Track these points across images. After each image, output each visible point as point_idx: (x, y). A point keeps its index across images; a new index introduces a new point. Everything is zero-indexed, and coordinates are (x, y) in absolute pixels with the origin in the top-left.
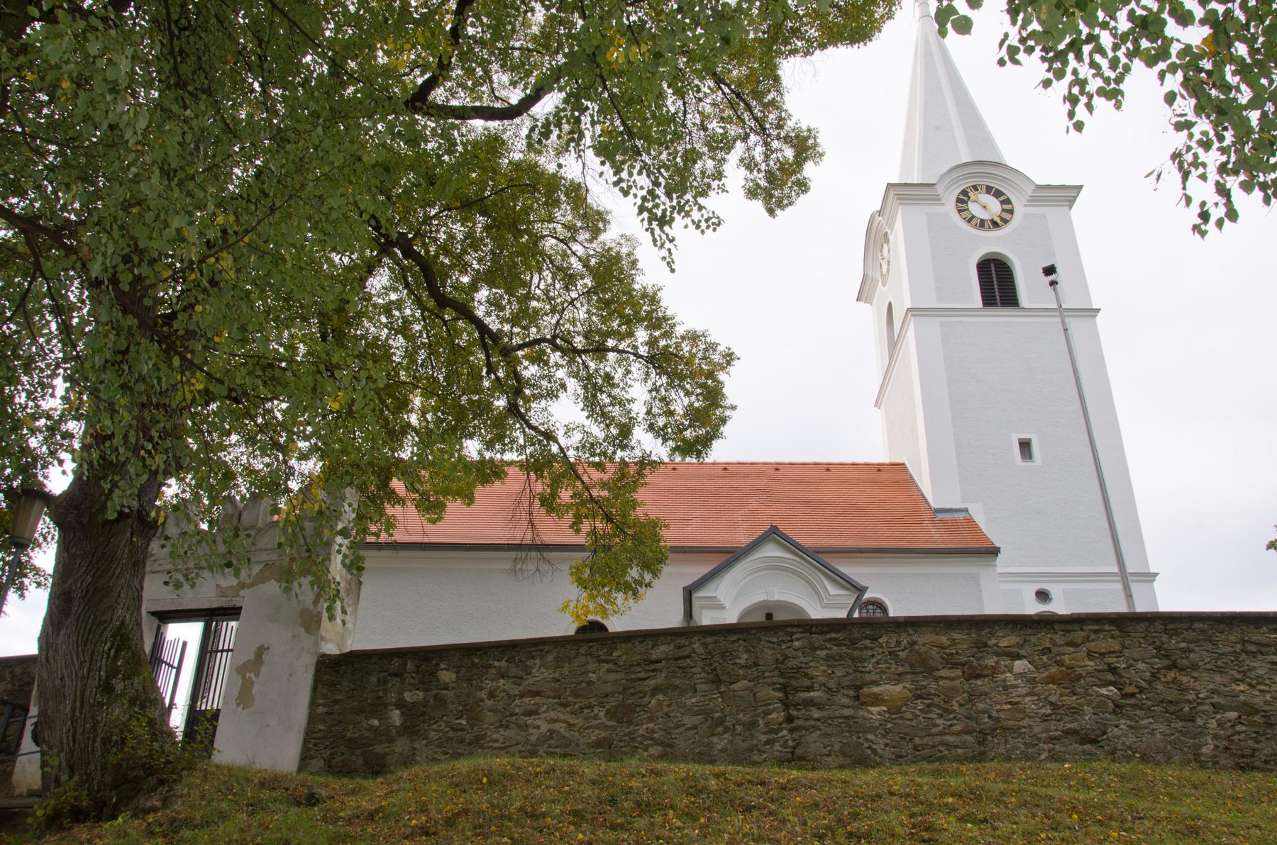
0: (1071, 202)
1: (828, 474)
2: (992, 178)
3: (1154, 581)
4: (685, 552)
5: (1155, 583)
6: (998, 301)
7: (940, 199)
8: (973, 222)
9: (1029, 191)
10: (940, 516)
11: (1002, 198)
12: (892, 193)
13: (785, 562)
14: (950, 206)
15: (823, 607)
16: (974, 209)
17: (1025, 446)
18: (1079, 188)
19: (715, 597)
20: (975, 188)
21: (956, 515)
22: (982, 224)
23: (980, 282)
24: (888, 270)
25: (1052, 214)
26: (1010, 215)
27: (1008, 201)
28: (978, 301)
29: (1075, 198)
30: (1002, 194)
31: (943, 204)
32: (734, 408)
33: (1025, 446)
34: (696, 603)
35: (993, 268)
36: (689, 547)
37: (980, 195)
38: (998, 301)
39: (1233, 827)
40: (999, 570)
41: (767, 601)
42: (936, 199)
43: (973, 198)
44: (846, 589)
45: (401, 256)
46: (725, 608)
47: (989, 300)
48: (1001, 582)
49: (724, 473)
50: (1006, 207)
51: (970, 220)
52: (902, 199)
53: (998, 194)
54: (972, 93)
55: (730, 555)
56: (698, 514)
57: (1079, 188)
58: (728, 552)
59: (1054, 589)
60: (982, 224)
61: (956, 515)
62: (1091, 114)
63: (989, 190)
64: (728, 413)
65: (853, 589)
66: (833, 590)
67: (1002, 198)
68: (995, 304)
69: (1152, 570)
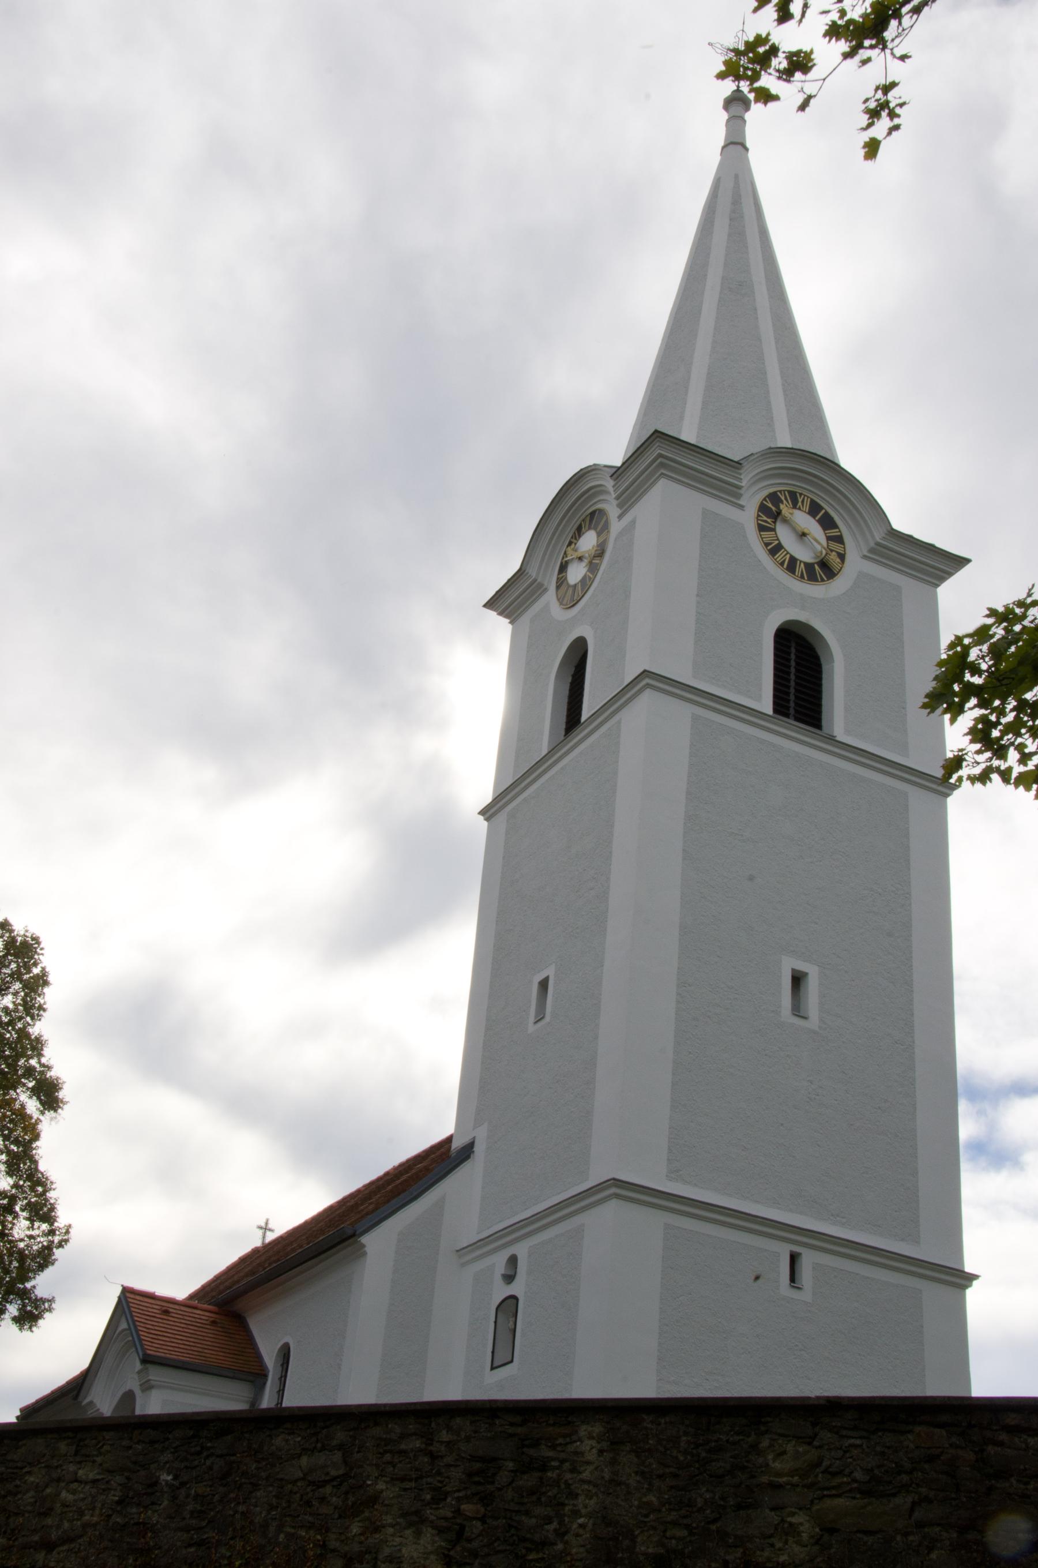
0: (942, 576)
2: (826, 491)
3: (948, 795)
5: (950, 800)
6: (792, 711)
7: (739, 496)
8: (779, 556)
9: (878, 536)
11: (833, 532)
14: (747, 517)
16: (784, 535)
22: (791, 565)
23: (776, 669)
25: (909, 586)
27: (839, 539)
28: (766, 704)
30: (835, 526)
31: (741, 507)
35: (793, 650)
37: (796, 512)
38: (792, 711)
42: (731, 493)
45: (992, 641)
47: (781, 706)
50: (834, 546)
51: (775, 549)
53: (827, 523)
54: (774, 245)
62: (920, 708)
63: (814, 509)
67: (833, 532)
68: (787, 715)
69: (968, 1268)
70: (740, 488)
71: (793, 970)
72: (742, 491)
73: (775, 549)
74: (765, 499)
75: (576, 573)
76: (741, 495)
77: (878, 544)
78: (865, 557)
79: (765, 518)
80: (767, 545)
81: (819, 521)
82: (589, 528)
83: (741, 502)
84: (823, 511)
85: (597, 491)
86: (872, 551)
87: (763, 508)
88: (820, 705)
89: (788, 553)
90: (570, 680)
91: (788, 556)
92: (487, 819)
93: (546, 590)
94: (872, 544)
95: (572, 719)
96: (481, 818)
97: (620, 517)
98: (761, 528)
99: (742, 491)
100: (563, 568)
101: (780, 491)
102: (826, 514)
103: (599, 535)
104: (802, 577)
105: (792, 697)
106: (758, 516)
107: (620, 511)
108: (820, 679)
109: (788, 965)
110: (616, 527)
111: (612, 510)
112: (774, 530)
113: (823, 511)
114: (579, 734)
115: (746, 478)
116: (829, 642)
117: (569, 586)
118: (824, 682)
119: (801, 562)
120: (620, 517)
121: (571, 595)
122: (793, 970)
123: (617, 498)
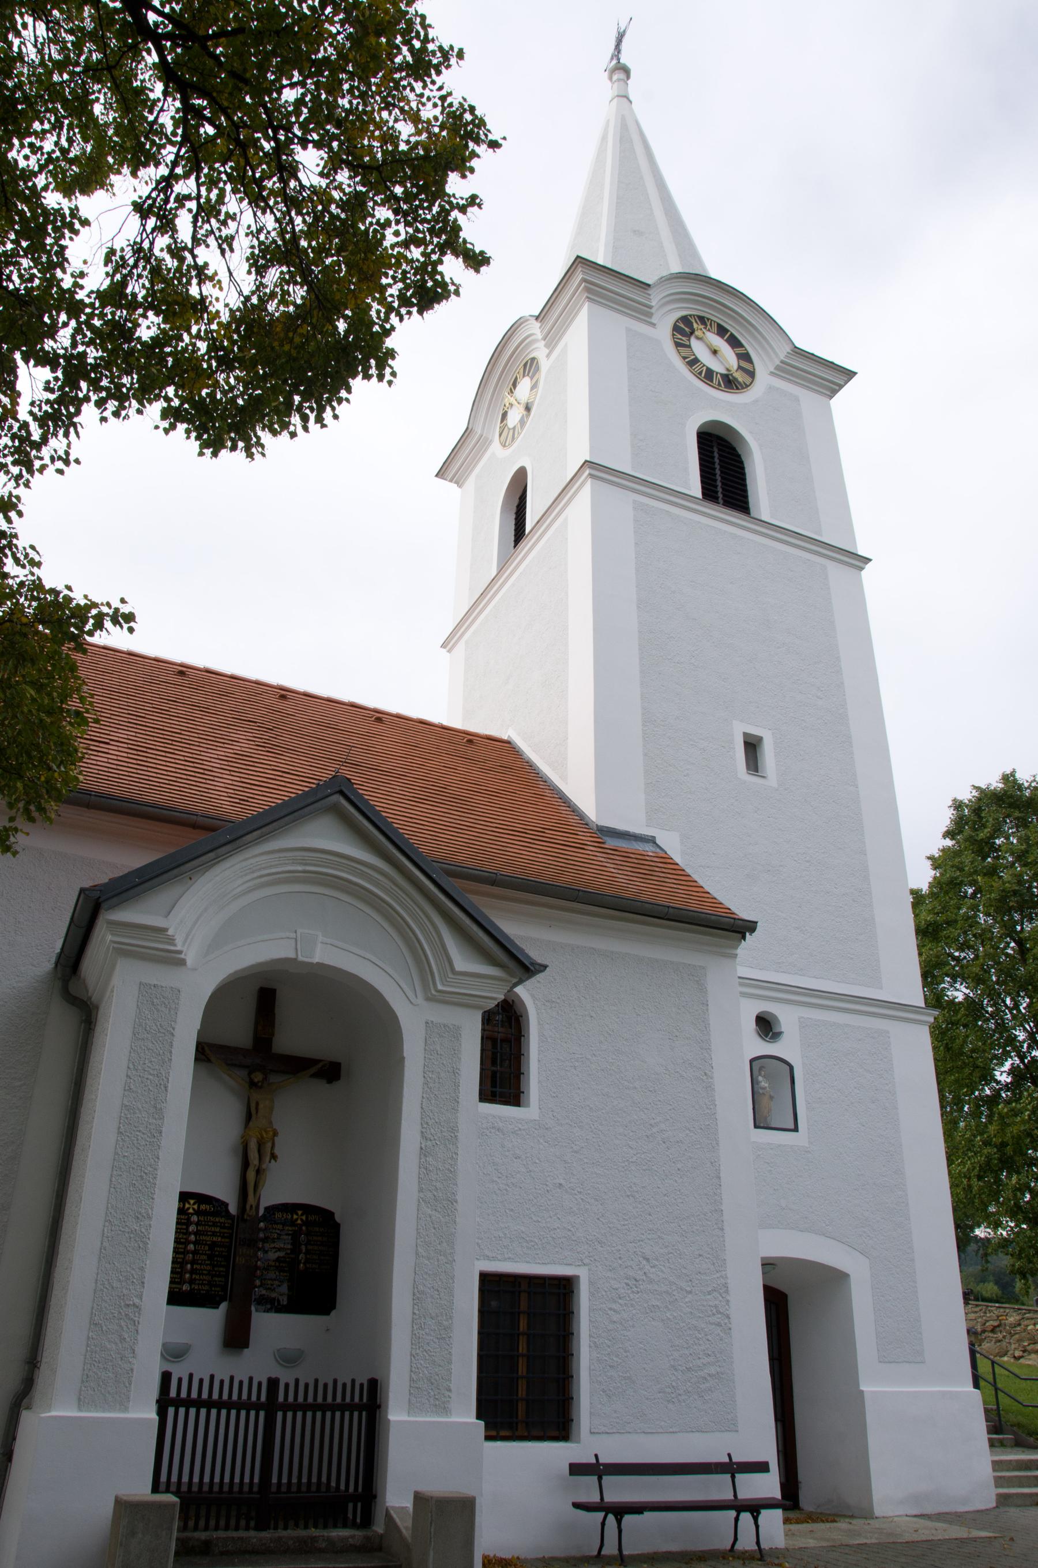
0: (833, 390)
1: (380, 727)
4: (88, 806)
7: (650, 315)
8: (697, 367)
9: (783, 351)
10: (611, 843)
12: (579, 276)
13: (363, 875)
14: (663, 332)
15: (428, 999)
16: (699, 349)
17: (752, 746)
18: (850, 374)
19: (163, 930)
20: (702, 320)
21: (640, 847)
22: (708, 376)
23: (700, 459)
24: (522, 422)
25: (807, 399)
26: (748, 380)
29: (837, 391)
30: (698, 375)
31: (653, 325)
32: (476, 261)
33: (752, 746)
34: (103, 938)
36: (100, 795)
38: (720, 495)
39: (626, 1283)
40: (743, 971)
41: (294, 960)
42: (644, 313)
43: (698, 333)
44: (492, 961)
46: (182, 963)
47: (709, 493)
48: (743, 995)
49: (179, 680)
50: (745, 365)
51: (693, 362)
52: (595, 293)
53: (734, 342)
55: (201, 836)
56: (122, 735)
57: (850, 374)
58: (195, 826)
59: (787, 1017)
60: (708, 376)
61: (640, 847)
63: (722, 331)
64: (451, 267)
65: (511, 964)
66: (463, 961)
70: (650, 307)
71: (745, 735)
72: (653, 310)
73: (693, 362)
74: (677, 321)
75: (514, 417)
76: (652, 314)
77: (782, 362)
78: (772, 374)
79: (680, 337)
80: (684, 358)
81: (726, 341)
82: (524, 376)
83: (653, 320)
84: (729, 334)
85: (527, 342)
86: (777, 368)
87: (676, 328)
88: (745, 485)
89: (704, 365)
90: (514, 516)
91: (705, 368)
92: (449, 651)
93: (491, 441)
94: (778, 362)
95: (519, 533)
96: (444, 651)
97: (548, 356)
98: (678, 345)
99: (653, 310)
100: (504, 416)
101: (690, 316)
102: (732, 335)
103: (532, 378)
104: (719, 384)
105: (719, 484)
106: (673, 335)
107: (547, 351)
108: (744, 480)
109: (738, 731)
110: (545, 364)
111: (540, 352)
112: (689, 346)
113: (729, 334)
114: (525, 545)
115: (655, 298)
116: (749, 441)
117: (509, 429)
118: (748, 482)
119: (717, 373)
120: (548, 356)
121: (508, 437)
122: (745, 735)
123: (544, 339)
